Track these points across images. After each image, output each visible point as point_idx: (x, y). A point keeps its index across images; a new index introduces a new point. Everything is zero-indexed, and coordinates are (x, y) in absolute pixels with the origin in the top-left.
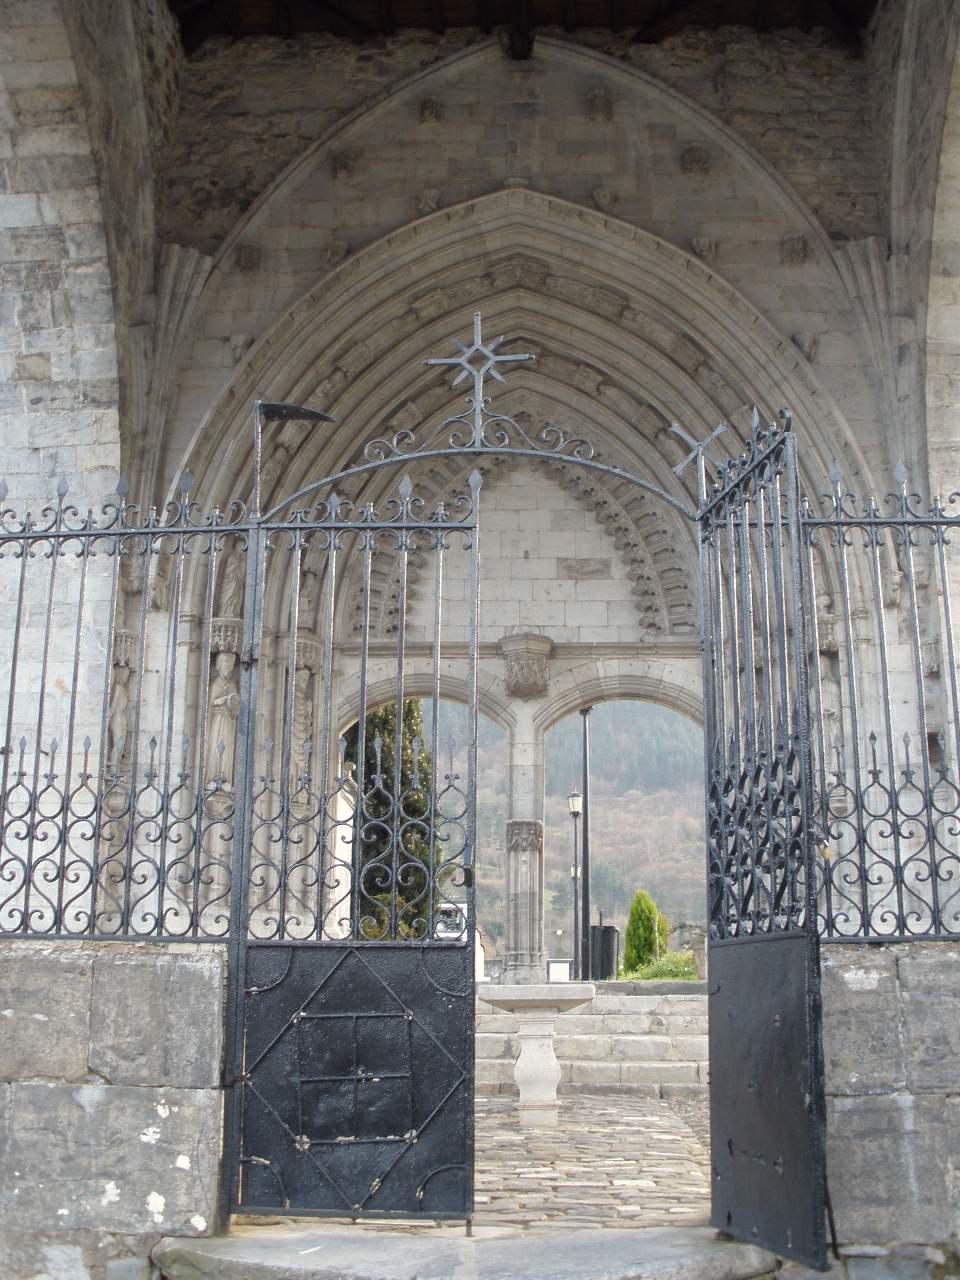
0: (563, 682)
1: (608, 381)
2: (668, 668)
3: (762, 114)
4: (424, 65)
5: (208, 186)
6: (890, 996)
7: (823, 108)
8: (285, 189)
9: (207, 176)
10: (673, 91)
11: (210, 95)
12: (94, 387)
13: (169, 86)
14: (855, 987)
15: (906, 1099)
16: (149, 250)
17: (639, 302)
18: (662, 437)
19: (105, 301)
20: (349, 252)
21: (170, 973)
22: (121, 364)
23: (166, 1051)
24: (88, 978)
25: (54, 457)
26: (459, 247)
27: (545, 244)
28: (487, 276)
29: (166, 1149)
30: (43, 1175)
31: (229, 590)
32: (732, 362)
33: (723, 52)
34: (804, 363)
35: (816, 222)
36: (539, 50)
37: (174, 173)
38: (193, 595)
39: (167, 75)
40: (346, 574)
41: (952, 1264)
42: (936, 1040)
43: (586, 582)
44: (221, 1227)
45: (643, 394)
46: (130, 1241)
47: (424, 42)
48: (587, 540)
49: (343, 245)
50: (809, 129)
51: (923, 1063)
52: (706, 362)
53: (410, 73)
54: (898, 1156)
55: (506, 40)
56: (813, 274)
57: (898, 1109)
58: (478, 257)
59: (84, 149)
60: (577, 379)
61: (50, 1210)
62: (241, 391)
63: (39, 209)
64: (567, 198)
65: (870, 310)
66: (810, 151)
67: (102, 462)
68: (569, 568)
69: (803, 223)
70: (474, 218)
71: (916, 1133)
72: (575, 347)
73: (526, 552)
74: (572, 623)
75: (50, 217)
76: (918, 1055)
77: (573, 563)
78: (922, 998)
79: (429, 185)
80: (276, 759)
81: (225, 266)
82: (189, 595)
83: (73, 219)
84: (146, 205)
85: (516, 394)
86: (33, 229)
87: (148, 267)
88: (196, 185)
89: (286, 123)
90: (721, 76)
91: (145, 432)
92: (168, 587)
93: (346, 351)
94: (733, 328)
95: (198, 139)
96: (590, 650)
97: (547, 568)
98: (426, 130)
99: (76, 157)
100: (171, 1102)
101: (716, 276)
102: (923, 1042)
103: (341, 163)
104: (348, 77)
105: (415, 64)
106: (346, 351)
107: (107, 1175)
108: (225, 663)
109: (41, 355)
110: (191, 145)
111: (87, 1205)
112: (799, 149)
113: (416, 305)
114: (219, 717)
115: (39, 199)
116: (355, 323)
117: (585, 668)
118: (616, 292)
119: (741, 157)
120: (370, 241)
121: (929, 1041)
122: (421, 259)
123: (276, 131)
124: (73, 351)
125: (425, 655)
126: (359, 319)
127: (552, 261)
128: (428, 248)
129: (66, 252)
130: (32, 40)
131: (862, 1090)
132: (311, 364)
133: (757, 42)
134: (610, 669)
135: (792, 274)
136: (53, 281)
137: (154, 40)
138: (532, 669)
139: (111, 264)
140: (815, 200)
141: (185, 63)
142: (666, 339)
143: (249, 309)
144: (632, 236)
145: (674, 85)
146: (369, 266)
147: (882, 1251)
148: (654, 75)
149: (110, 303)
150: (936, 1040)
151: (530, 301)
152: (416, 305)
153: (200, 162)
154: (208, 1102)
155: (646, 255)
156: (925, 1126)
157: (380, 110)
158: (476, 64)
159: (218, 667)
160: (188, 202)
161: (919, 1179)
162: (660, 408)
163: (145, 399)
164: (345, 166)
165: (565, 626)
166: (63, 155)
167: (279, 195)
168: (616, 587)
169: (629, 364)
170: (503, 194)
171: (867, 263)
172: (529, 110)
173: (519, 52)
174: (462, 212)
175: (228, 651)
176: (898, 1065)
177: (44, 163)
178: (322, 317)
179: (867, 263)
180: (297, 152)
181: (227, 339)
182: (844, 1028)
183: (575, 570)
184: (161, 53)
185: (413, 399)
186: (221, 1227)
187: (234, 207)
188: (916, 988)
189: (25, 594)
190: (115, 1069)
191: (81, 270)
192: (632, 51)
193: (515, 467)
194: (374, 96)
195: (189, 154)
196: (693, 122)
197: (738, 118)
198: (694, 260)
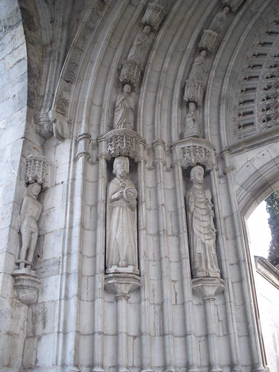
12: (9, 19)
40: (222, 102)
67: (18, 59)
80: (182, 241)
91: (52, 42)
114: (117, 208)
116: (234, 337)
159: (114, 171)
163: (50, 25)
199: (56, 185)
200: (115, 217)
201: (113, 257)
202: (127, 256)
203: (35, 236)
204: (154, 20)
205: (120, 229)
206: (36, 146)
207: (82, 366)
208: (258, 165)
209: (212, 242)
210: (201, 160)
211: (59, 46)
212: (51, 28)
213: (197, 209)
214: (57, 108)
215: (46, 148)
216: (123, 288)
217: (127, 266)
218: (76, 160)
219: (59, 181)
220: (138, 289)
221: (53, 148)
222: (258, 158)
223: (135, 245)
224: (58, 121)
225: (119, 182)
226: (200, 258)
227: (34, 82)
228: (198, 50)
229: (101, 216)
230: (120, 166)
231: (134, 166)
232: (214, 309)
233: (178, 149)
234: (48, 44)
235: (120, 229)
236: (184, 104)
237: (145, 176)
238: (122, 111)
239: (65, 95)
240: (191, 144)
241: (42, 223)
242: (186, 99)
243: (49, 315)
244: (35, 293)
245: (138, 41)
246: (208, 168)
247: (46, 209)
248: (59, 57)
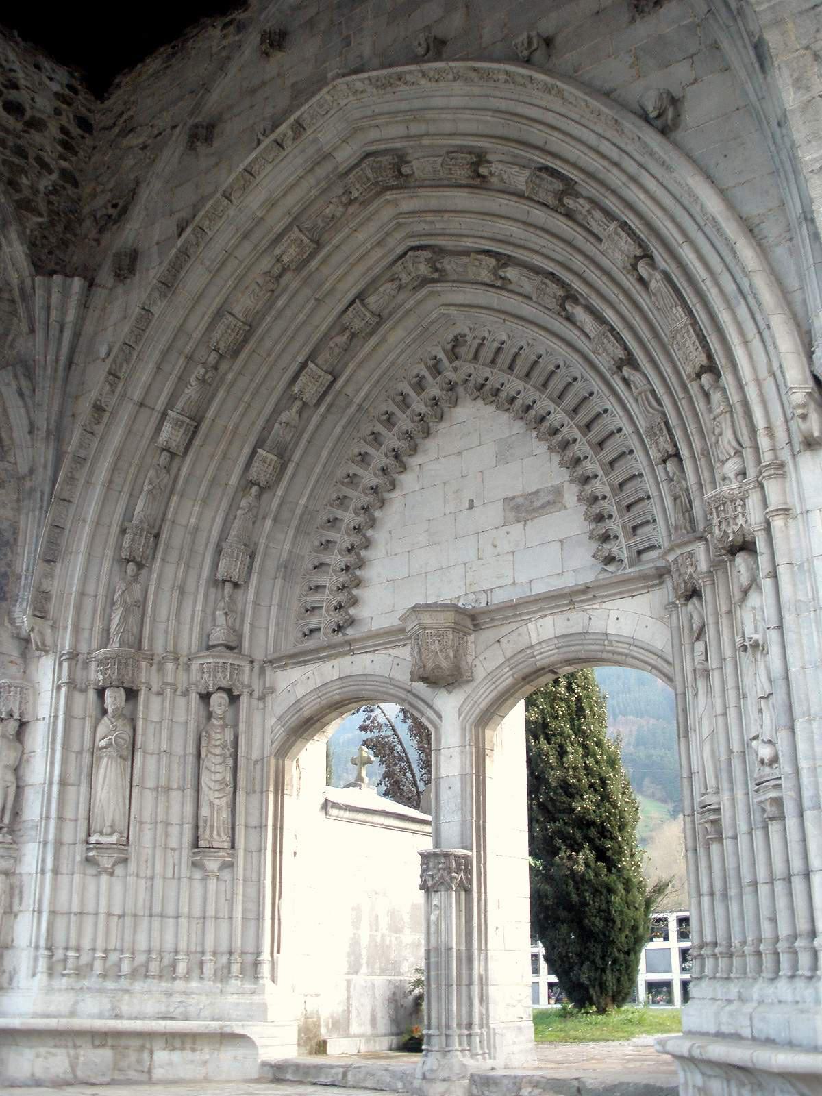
2: (613, 615)
8: (157, 185)
9: (109, 201)
43: (536, 520)
45: (538, 261)
48: (538, 468)
52: (570, 188)
68: (517, 508)
72: (461, 236)
73: (471, 501)
74: (522, 578)
77: (520, 500)
91: (32, 471)
92: (53, 627)
96: (514, 610)
97: (492, 514)
114: (105, 760)
117: (515, 634)
122: (272, 204)
125: (347, 653)
144: (451, 76)
165: (514, 583)
168: (570, 521)
169: (516, 231)
174: (290, 133)
183: (524, 509)
189: (789, 652)
199: (37, 719)
200: (102, 771)
201: (96, 825)
202: (113, 821)
203: (12, 791)
204: (174, 444)
205: (106, 787)
206: (13, 658)
207: (57, 948)
208: (300, 691)
210: (224, 684)
211: (42, 477)
212: (29, 444)
213: (209, 755)
214: (35, 609)
215: (28, 656)
216: (106, 862)
217: (111, 834)
218: (59, 688)
219: (40, 716)
221: (35, 660)
222: (302, 682)
223: (124, 804)
224: (36, 629)
225: (109, 722)
226: (205, 822)
227: (5, 555)
228: (247, 484)
229: (86, 770)
230: (113, 699)
231: (132, 694)
233: (195, 665)
234: (26, 475)
235: (106, 787)
238: (120, 611)
239: (46, 585)
240: (211, 660)
241: (21, 772)
242: (219, 576)
243: (26, 890)
244: (12, 861)
245: (150, 483)
246: (236, 693)
247: (26, 751)
248: (42, 500)
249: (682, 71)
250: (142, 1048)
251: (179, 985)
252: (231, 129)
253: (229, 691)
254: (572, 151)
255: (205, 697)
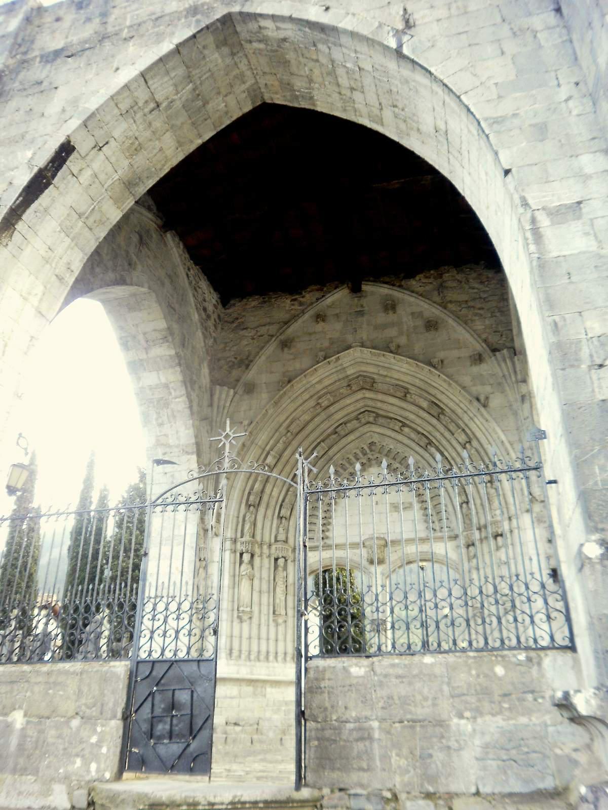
0: (393, 556)
1: (404, 425)
3: (459, 302)
4: (318, 299)
5: (233, 360)
6: (369, 679)
7: (485, 296)
8: (263, 358)
10: (420, 297)
11: (233, 322)
13: (215, 321)
14: (355, 675)
15: (375, 724)
16: (208, 388)
17: (413, 390)
18: (428, 446)
19: (187, 412)
20: (289, 382)
21: (106, 673)
22: (196, 437)
23: (102, 705)
24: (78, 677)
25: (173, 476)
26: (335, 375)
27: (371, 369)
28: (349, 385)
29: (99, 745)
30: (56, 756)
31: (247, 527)
32: (453, 411)
33: (441, 277)
34: (482, 409)
35: (485, 346)
36: (364, 287)
37: (220, 355)
38: (232, 529)
39: (214, 317)
41: (394, 798)
42: (389, 698)
44: (119, 776)
45: (419, 429)
46: (83, 783)
47: (317, 290)
49: (286, 379)
50: (479, 306)
51: (383, 708)
53: (312, 304)
54: (372, 750)
55: (350, 285)
56: (484, 369)
57: (372, 729)
58: (343, 378)
59: (173, 352)
60: (391, 426)
61: (57, 770)
62: (248, 443)
63: (159, 378)
64: (378, 349)
65: (509, 381)
66: (481, 315)
69: (479, 347)
70: (340, 362)
71: (380, 739)
75: (163, 380)
76: (381, 704)
78: (382, 679)
79: (321, 351)
81: (240, 391)
82: (229, 529)
83: (172, 380)
84: (205, 371)
85: (368, 435)
86: (157, 385)
87: (207, 396)
88: (228, 360)
89: (263, 330)
90: (441, 288)
93: (292, 423)
94: (452, 396)
95: (228, 341)
98: (320, 326)
99: (170, 356)
100: (103, 726)
101: (441, 375)
102: (383, 698)
103: (285, 344)
104: (287, 308)
105: (314, 299)
106: (292, 423)
107: (77, 755)
108: (246, 557)
109: (165, 435)
110: (226, 343)
111: (70, 768)
112: (476, 315)
113: (320, 401)
115: (158, 374)
118: (403, 387)
119: (450, 321)
120: (296, 377)
121: (385, 698)
122: (319, 382)
123: (259, 334)
124: (177, 432)
126: (296, 410)
127: (375, 376)
128: (323, 376)
129: (170, 393)
130: (149, 314)
131: (357, 720)
132: (277, 431)
133: (455, 272)
134: (411, 549)
135: (475, 369)
136: (167, 405)
137: (206, 304)
138: (379, 551)
139: (189, 396)
140: (484, 336)
141: (223, 310)
142: (425, 404)
143: (250, 410)
145: (421, 295)
146: (299, 385)
147: (364, 792)
148: (413, 292)
149: (189, 412)
150: (389, 698)
151: (368, 394)
152: (320, 401)
153: (230, 350)
154: (115, 726)
155: (413, 369)
156: (383, 736)
157: (300, 321)
158: (339, 296)
160: (225, 367)
161: (381, 761)
162: (427, 434)
164: (286, 346)
166: (165, 355)
167: (261, 361)
168: (416, 512)
169: (412, 417)
170: (351, 351)
171: (504, 360)
172: (361, 313)
173: (356, 289)
175: (247, 552)
176: (372, 709)
177: (159, 359)
178: (280, 410)
179: (504, 360)
180: (268, 342)
181: (241, 423)
182: (350, 693)
184: (210, 308)
185: (323, 441)
186: (119, 776)
187: (244, 367)
188: (381, 674)
190: (84, 713)
191: (177, 400)
192: (403, 283)
193: (370, 466)
194: (298, 315)
195: (225, 347)
196: (430, 310)
197: (449, 305)
198: (432, 370)
201: (241, 604)
209: (283, 598)
210: (284, 555)
220: (251, 618)
230: (246, 557)
231: (252, 556)
232: (281, 629)
233: (273, 547)
236: (280, 518)
237: (257, 560)
242: (281, 515)
249: (488, 389)
250: (262, 687)
251: (271, 664)
252: (300, 346)
253: (285, 558)
254: (446, 401)
255: (276, 560)
